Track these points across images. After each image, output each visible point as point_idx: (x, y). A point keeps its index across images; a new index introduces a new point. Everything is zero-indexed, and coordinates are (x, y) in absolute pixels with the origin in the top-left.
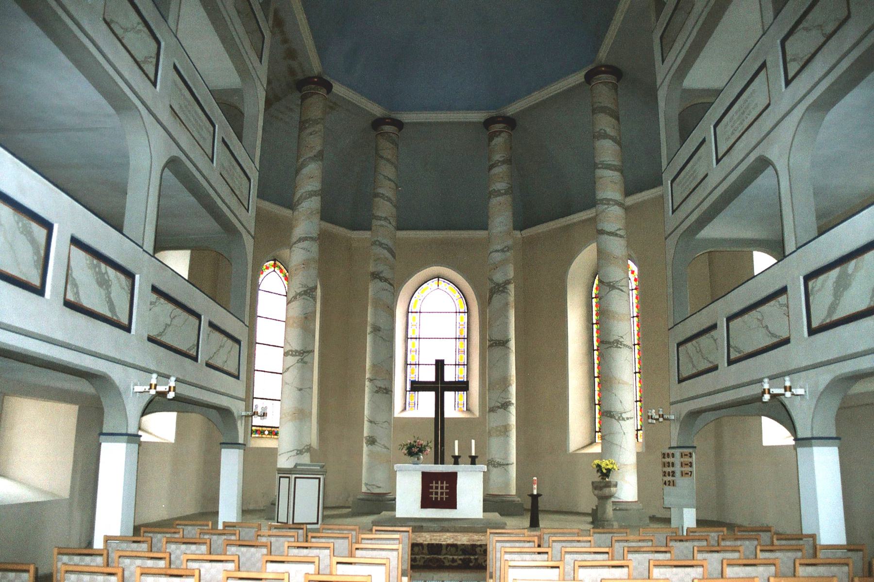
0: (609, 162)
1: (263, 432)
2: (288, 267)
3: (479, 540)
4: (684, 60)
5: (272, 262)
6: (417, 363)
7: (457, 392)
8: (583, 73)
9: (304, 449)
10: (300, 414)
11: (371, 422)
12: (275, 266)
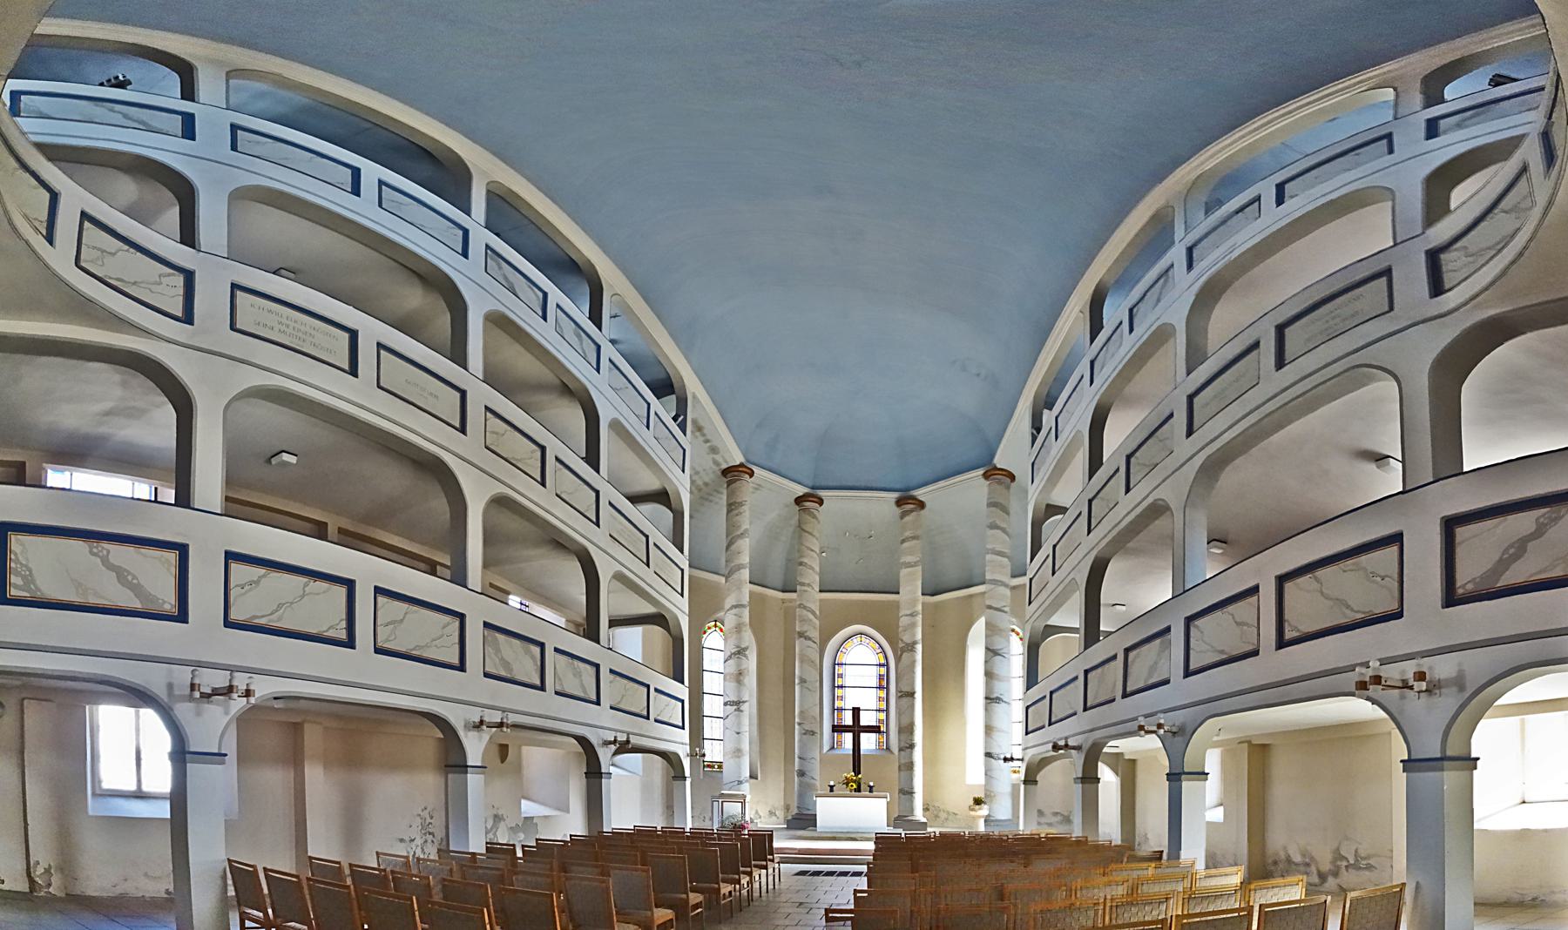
8: (982, 472)
11: (800, 758)
12: (716, 626)
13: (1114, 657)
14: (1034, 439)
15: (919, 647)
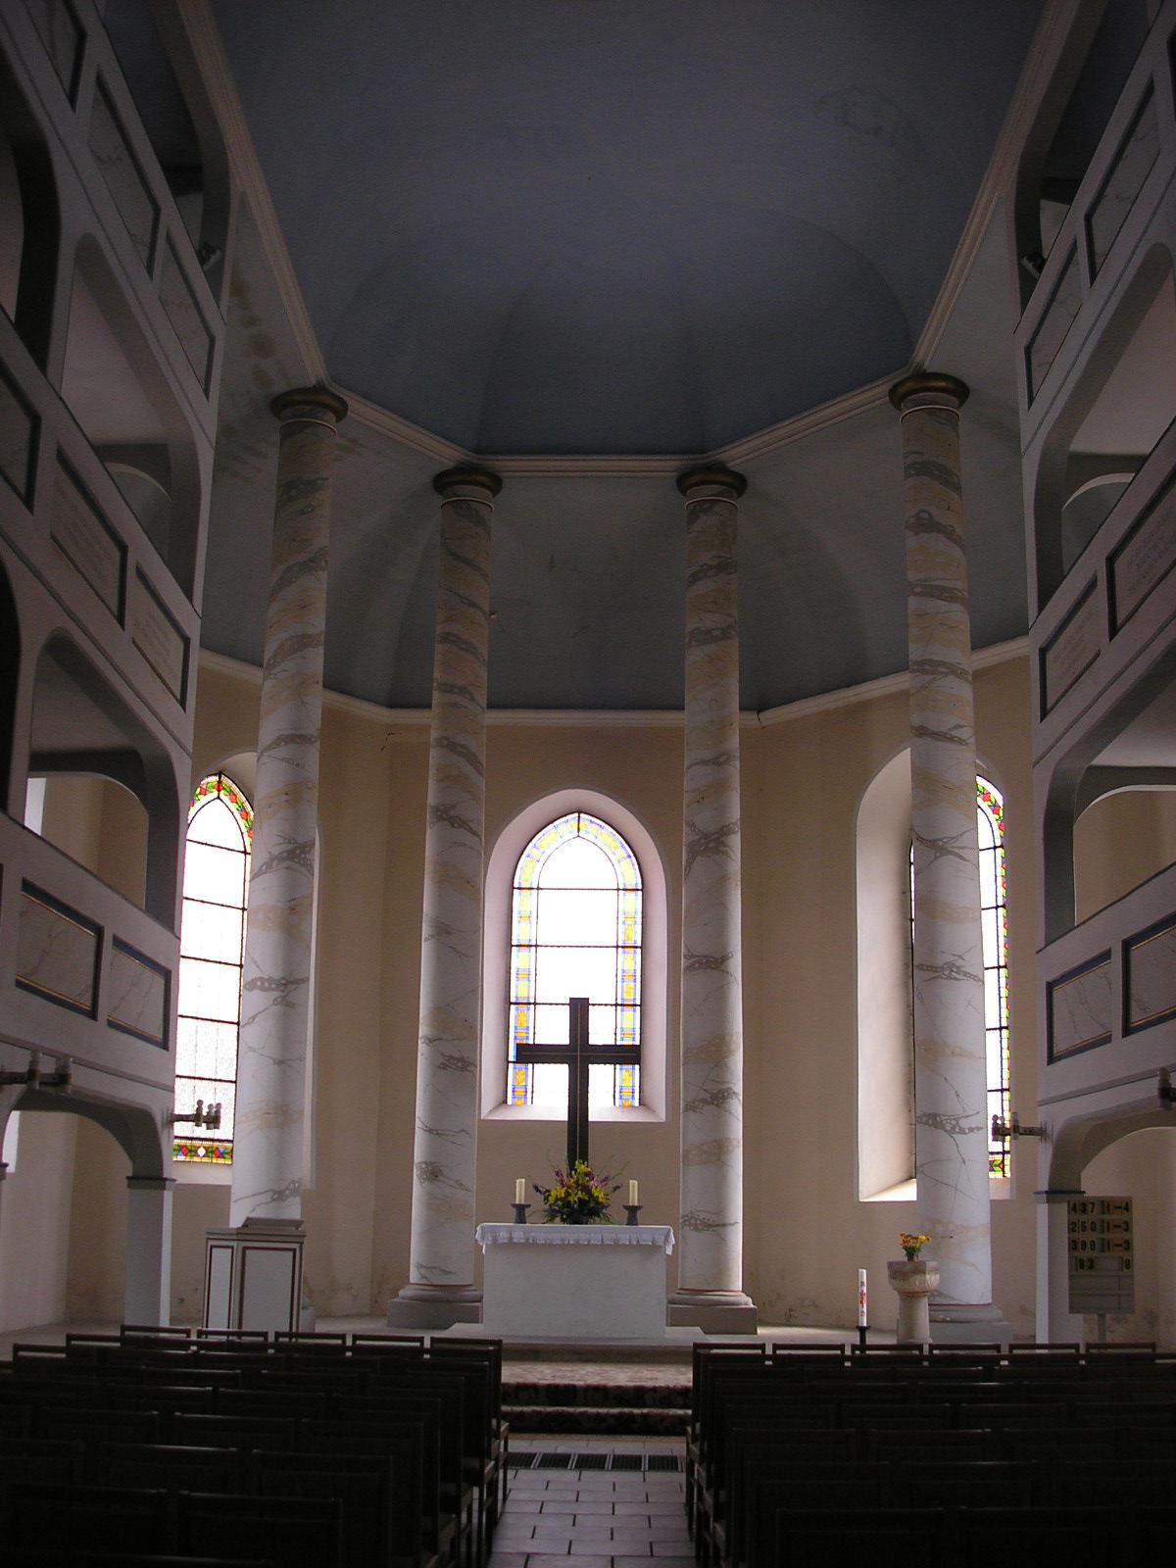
0: (937, 583)
1: (193, 1152)
2: (253, 796)
3: (652, 1379)
4: (1075, 395)
5: (214, 779)
6: (532, 1001)
7: (618, 1066)
8: (887, 387)
9: (287, 1189)
10: (279, 1115)
12: (219, 787)
13: (1106, 955)
14: (1027, 285)
15: (735, 842)
